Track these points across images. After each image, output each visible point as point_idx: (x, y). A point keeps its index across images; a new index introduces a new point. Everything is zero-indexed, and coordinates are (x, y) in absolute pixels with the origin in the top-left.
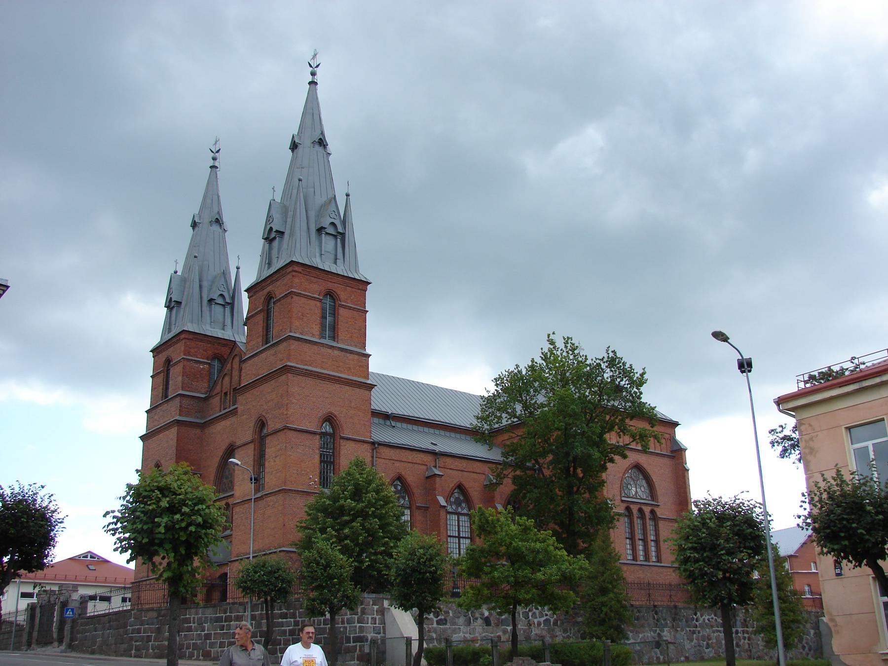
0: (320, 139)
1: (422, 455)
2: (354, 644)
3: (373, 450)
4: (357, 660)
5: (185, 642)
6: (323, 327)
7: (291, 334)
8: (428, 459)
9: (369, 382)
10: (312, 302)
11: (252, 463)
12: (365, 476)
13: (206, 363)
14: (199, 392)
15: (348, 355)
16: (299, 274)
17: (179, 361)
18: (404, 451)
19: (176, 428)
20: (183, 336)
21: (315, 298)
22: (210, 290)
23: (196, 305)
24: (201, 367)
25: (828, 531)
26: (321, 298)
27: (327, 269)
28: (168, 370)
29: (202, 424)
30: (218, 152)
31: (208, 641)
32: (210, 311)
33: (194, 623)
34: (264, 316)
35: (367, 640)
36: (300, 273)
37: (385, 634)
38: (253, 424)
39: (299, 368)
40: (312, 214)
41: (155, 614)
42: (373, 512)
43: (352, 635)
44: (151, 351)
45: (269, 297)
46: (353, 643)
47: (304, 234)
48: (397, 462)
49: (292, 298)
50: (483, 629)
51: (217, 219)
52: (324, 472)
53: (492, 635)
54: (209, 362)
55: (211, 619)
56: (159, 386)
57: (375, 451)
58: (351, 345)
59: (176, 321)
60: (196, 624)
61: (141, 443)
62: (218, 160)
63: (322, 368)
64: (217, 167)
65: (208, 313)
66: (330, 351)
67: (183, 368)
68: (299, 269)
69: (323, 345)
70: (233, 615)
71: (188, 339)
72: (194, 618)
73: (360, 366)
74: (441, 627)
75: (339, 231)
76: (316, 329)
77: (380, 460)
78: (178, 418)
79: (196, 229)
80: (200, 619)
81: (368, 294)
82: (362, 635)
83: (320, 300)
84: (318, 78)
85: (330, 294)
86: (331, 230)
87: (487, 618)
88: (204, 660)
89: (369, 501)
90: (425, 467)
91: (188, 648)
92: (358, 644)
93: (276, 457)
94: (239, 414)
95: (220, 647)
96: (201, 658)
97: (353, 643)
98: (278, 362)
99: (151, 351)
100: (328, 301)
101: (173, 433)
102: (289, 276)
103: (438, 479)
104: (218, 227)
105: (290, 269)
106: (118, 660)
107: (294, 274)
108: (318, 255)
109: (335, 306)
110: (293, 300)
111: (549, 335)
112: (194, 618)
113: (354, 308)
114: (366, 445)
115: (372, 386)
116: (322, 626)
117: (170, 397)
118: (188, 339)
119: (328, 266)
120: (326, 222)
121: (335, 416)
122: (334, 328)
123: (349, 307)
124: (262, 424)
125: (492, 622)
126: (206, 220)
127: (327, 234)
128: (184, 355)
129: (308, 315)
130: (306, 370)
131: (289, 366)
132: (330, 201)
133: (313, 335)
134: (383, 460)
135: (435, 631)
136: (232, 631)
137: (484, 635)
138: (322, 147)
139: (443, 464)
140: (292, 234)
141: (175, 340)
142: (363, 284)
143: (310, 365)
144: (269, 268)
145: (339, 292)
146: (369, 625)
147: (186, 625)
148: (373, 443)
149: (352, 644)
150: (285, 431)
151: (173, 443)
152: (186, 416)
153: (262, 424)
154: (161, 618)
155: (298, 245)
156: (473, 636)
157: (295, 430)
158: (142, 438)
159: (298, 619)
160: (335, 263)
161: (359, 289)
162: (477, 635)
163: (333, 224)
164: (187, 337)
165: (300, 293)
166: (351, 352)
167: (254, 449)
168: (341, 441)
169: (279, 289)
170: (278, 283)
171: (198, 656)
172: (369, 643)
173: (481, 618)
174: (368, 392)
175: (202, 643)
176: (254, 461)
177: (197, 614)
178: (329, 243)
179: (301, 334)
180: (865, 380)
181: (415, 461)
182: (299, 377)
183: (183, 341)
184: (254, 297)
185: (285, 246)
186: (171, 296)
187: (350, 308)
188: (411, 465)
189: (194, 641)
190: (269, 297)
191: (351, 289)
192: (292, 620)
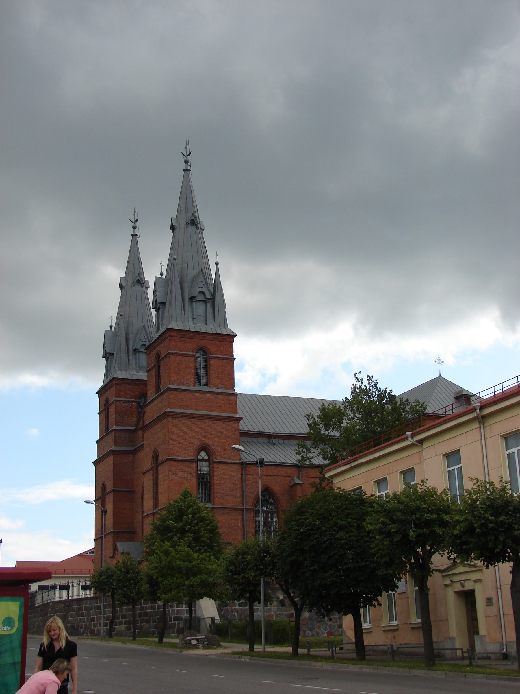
0: (192, 220)
1: (286, 469)
2: (174, 622)
3: (242, 469)
4: (176, 633)
5: (80, 624)
6: (197, 376)
7: (170, 386)
8: (290, 471)
9: (238, 416)
10: (187, 359)
11: (152, 486)
12: (186, 503)
13: (134, 402)
14: (129, 426)
15: (219, 396)
16: (175, 338)
17: (113, 403)
18: (270, 467)
19: (112, 456)
20: (114, 382)
21: (189, 355)
22: (134, 341)
23: (124, 356)
24: (130, 405)
25: (218, 570)
26: (194, 354)
27: (198, 330)
28: (108, 409)
29: (133, 451)
30: (137, 221)
31: (93, 623)
32: (136, 359)
33: (85, 611)
34: (156, 370)
35: (181, 619)
36: (176, 337)
37: (196, 614)
38: (152, 455)
39: (176, 413)
40: (186, 285)
41: (63, 605)
42: (190, 528)
43: (173, 616)
44: (96, 393)
45: (158, 356)
46: (174, 621)
47: (179, 304)
48: (264, 476)
49: (170, 357)
50: (278, 609)
51: (138, 280)
52: (205, 490)
53: (286, 613)
54: (137, 400)
55: (94, 607)
56: (103, 422)
57: (244, 470)
58: (222, 388)
59: (110, 369)
60: (86, 611)
61: (94, 467)
62: (137, 229)
63: (197, 409)
64: (137, 235)
65: (134, 361)
66: (202, 395)
67: (116, 408)
68: (175, 334)
69: (197, 391)
70: (107, 604)
71: (117, 384)
72: (85, 607)
73: (230, 404)
74: (242, 608)
75: (207, 297)
76: (191, 379)
77: (249, 476)
78: (113, 448)
79: (123, 290)
80: (88, 607)
81: (235, 344)
82: (178, 615)
83: (193, 356)
84: (193, 166)
85: (202, 349)
86: (202, 298)
87: (282, 600)
88: (91, 636)
89: (186, 521)
90: (290, 478)
91: (82, 628)
92: (176, 622)
93: (163, 481)
94: (144, 447)
95: (99, 627)
96: (89, 634)
97: (174, 621)
98: (163, 408)
99: (96, 393)
100: (201, 355)
101: (111, 459)
102: (167, 340)
103: (298, 488)
104: (140, 286)
105: (168, 335)
106: (34, 638)
107: (170, 338)
108: (190, 319)
109: (207, 358)
110: (170, 359)
111: (355, 375)
112: (85, 607)
113: (223, 358)
114: (236, 466)
115: (240, 419)
116: (156, 610)
117: (109, 431)
118: (117, 384)
119: (201, 327)
120: (196, 292)
121: (209, 446)
122: (207, 376)
123: (218, 357)
124: (156, 455)
125: (286, 603)
126: (130, 283)
127: (197, 301)
128: (116, 397)
129: (184, 369)
130: (183, 413)
131: (167, 412)
132: (199, 273)
133: (189, 385)
134: (252, 476)
135: (237, 612)
136: (106, 615)
137: (279, 613)
138: (195, 226)
139: (306, 474)
140: (170, 304)
141: (109, 385)
142: (232, 337)
143: (187, 409)
144: (157, 332)
145: (209, 347)
146: (184, 608)
147: (81, 612)
148: (242, 464)
149: (173, 622)
150: (168, 462)
151: (111, 467)
152: (120, 446)
153: (156, 455)
154: (66, 608)
155: (174, 314)
156: (269, 614)
157: (175, 460)
158: (95, 463)
159: (143, 605)
160: (206, 324)
161: (227, 342)
162: (273, 613)
163: (201, 292)
164: (117, 383)
165: (176, 353)
166: (221, 394)
167: (153, 474)
168: (215, 465)
169: (163, 349)
170: (162, 345)
171: (87, 633)
172: (183, 621)
173: (276, 601)
174: (237, 424)
175: (89, 624)
176: (153, 484)
177: (86, 604)
178: (199, 308)
179: (179, 385)
180: (352, 462)
181: (280, 474)
182: (177, 419)
183: (114, 386)
184: (150, 355)
185: (166, 314)
186: (106, 349)
187: (219, 358)
188: (277, 478)
189: (85, 623)
190: (158, 356)
191: (220, 342)
192: (140, 606)
